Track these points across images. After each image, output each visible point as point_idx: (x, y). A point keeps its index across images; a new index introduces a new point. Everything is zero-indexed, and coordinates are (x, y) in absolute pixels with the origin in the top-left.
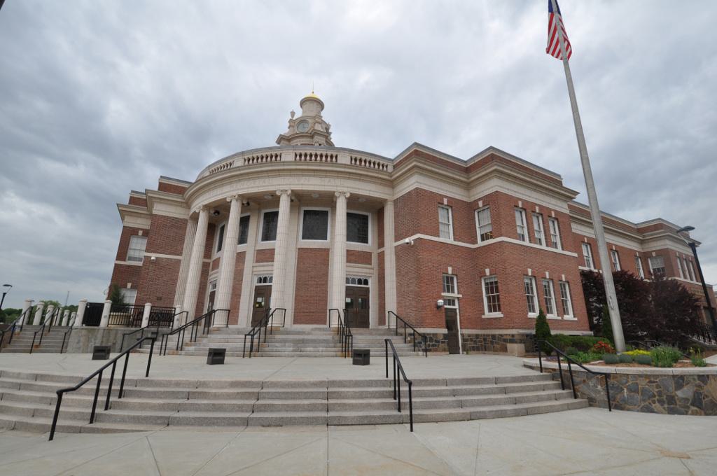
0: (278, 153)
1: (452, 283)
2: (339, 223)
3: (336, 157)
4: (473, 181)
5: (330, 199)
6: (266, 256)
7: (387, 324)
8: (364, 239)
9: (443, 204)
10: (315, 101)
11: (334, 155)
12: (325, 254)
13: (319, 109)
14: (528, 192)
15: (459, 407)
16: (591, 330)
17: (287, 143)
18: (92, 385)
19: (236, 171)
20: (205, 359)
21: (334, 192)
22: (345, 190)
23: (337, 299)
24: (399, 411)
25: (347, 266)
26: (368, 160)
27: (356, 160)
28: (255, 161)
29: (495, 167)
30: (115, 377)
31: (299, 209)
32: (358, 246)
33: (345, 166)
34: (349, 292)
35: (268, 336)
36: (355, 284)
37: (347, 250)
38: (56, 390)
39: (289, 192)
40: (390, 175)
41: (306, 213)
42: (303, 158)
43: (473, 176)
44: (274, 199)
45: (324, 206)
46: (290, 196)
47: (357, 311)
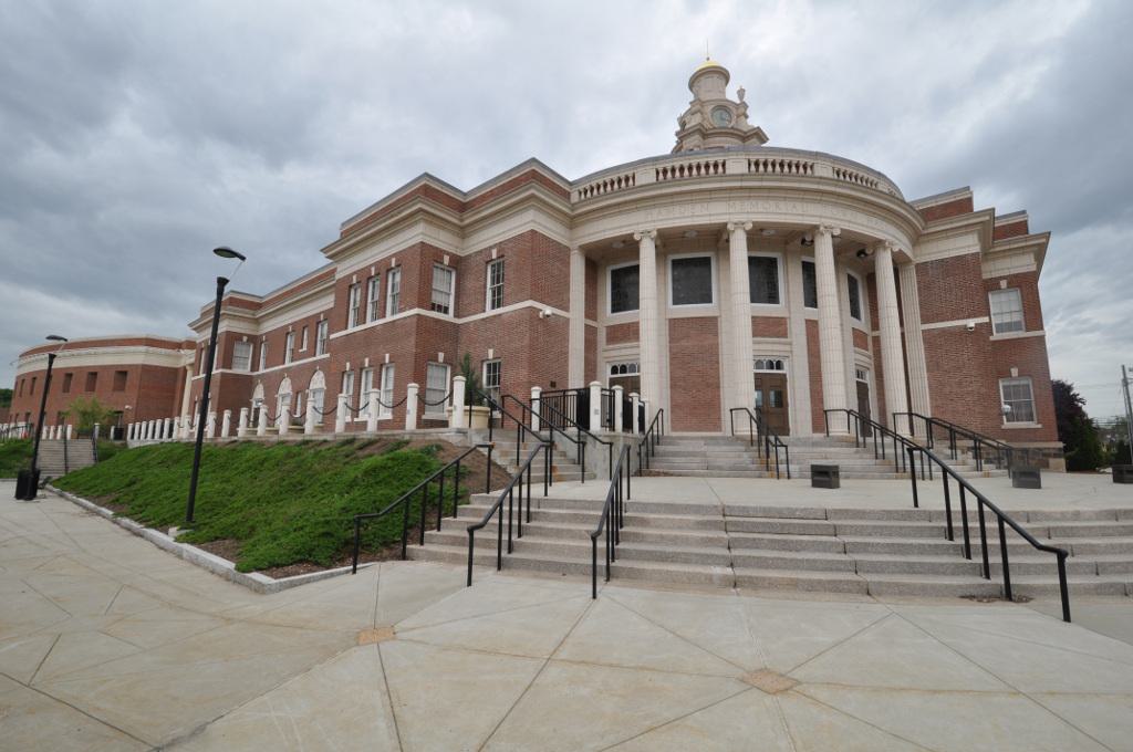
0: (630, 174)
1: (489, 378)
2: (736, 272)
3: (724, 165)
4: (580, 215)
5: (717, 238)
6: (629, 333)
7: (675, 434)
8: (773, 298)
9: (442, 263)
10: (704, 73)
11: (694, 165)
12: (709, 325)
13: (724, 82)
14: (748, 205)
15: (1092, 573)
16: (1060, 440)
17: (740, 143)
18: (494, 520)
19: (828, 184)
20: (809, 482)
21: (726, 224)
22: (743, 218)
23: (740, 393)
24: (988, 577)
25: (754, 343)
26: (794, 162)
27: (757, 164)
28: (595, 191)
29: (532, 191)
30: (952, 508)
31: (666, 256)
32: (766, 309)
33: (741, 177)
34: (760, 382)
35: (651, 458)
36: (762, 368)
37: (753, 317)
38: (466, 526)
39: (655, 233)
40: (573, 207)
41: (676, 263)
42: (677, 174)
43: (467, 218)
44: (630, 246)
45: (705, 251)
46: (655, 239)
47: (772, 415)
